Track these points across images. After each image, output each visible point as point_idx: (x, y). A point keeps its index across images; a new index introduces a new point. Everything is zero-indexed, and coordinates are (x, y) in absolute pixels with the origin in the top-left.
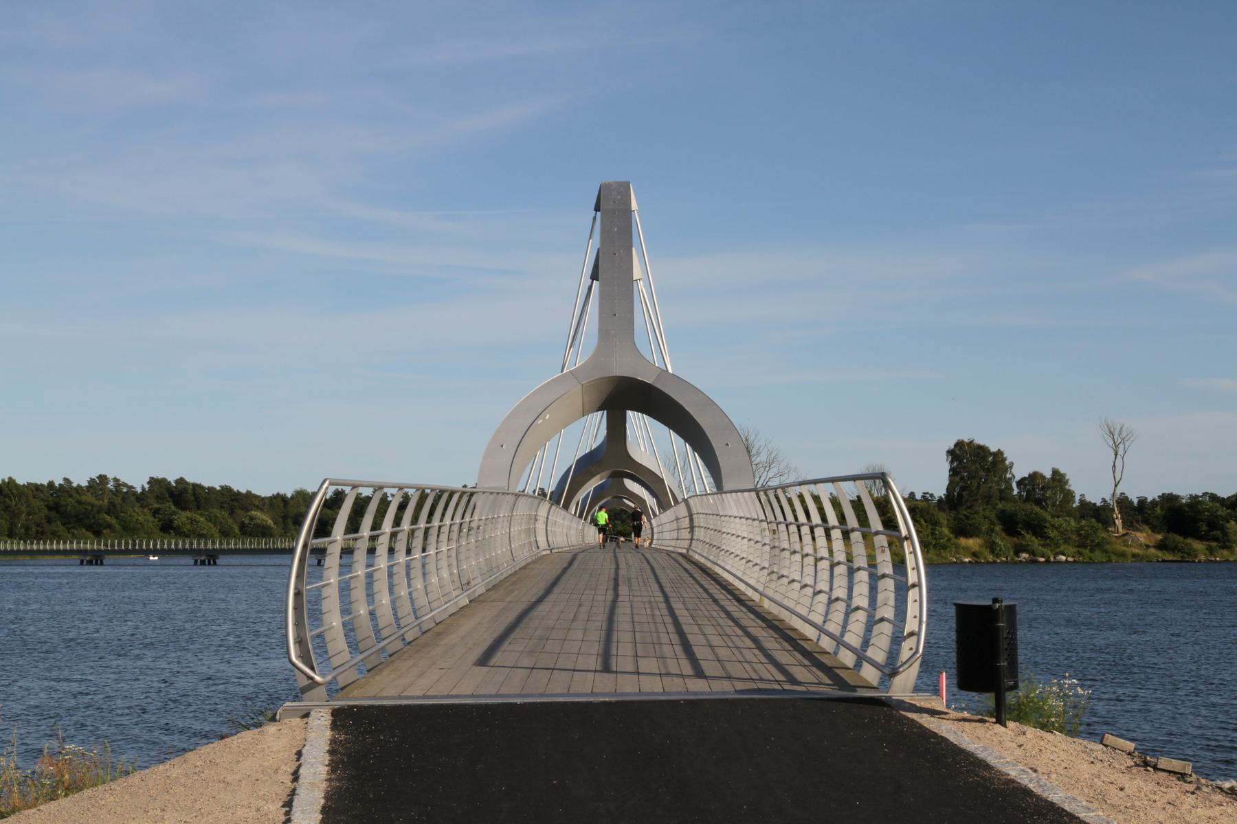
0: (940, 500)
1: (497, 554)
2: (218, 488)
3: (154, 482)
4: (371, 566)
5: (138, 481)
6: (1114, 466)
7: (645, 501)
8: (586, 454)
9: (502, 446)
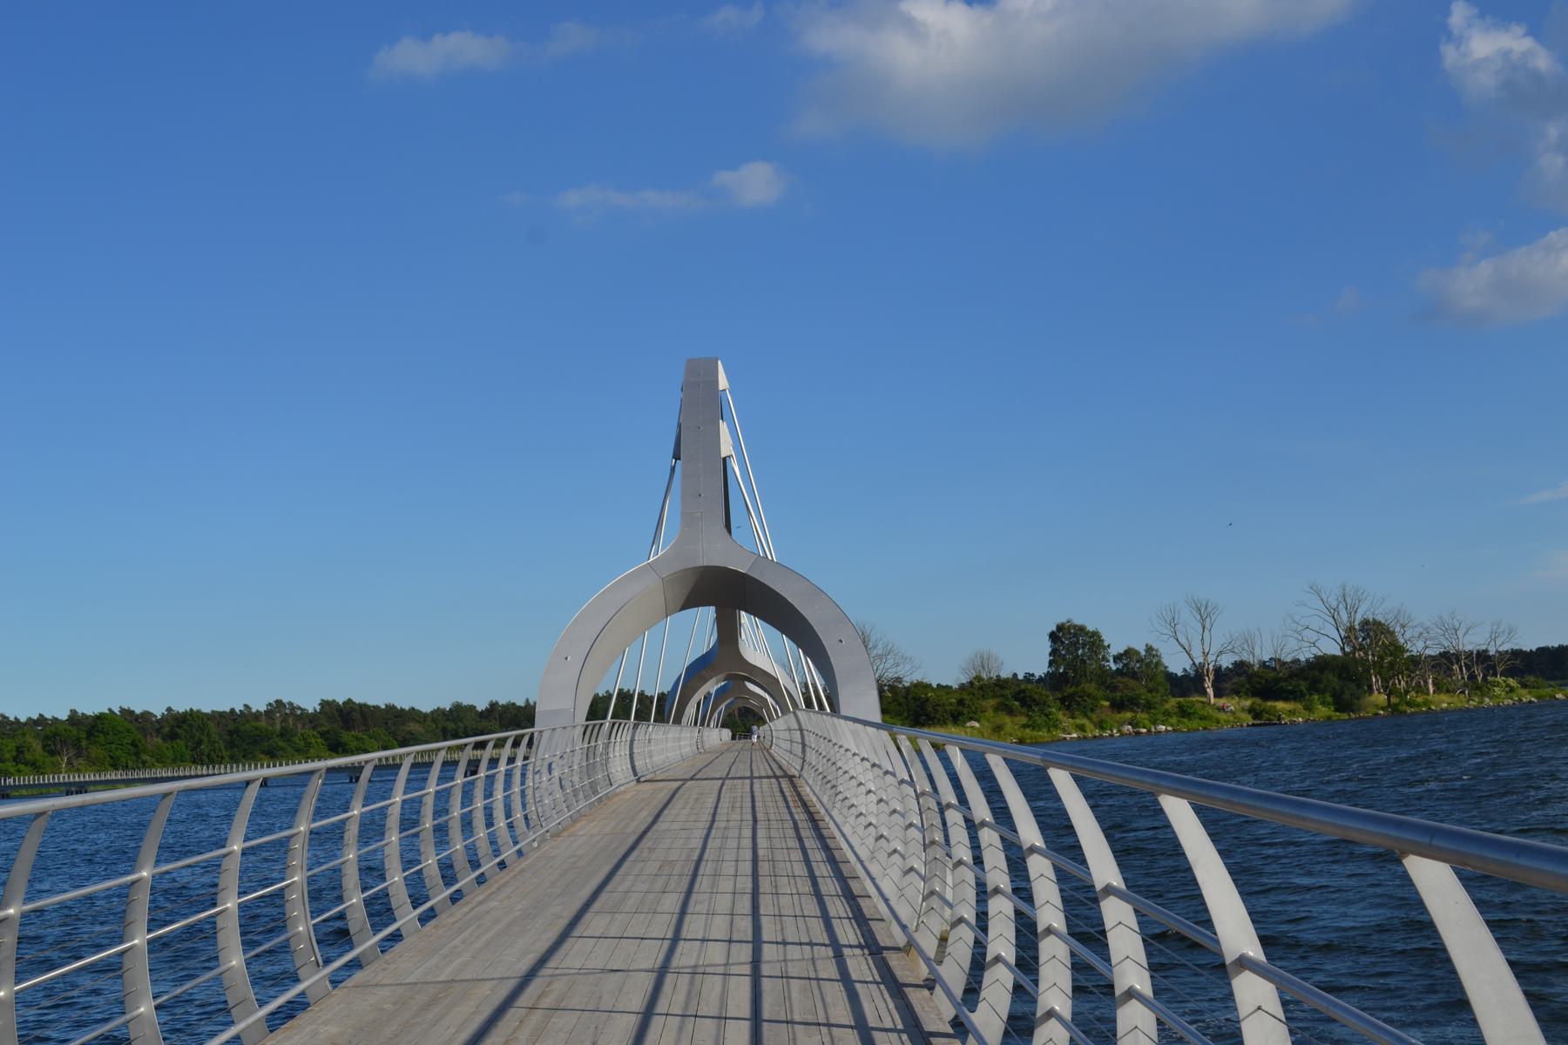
0: (1041, 679)
2: (383, 707)
3: (325, 704)
5: (311, 704)
6: (1203, 639)
8: (703, 655)
9: (566, 659)
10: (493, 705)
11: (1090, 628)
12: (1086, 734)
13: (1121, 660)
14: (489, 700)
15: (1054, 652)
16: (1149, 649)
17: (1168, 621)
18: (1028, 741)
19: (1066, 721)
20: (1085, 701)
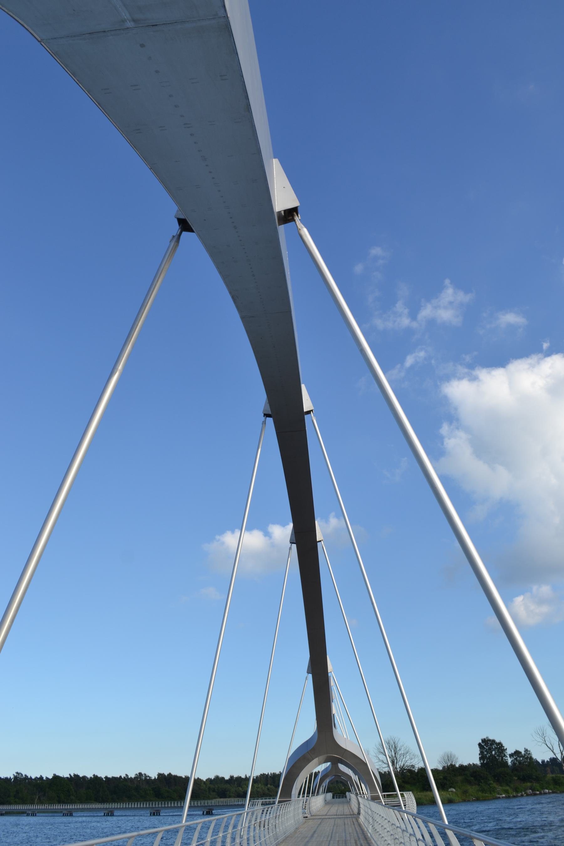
1: (285, 826)
2: (184, 777)
4: (202, 839)
7: (351, 777)
10: (232, 777)
11: (497, 741)
12: (510, 795)
13: (513, 756)
14: (230, 775)
15: (481, 753)
16: (526, 750)
17: (541, 736)
18: (481, 799)
19: (499, 788)
20: (506, 777)
